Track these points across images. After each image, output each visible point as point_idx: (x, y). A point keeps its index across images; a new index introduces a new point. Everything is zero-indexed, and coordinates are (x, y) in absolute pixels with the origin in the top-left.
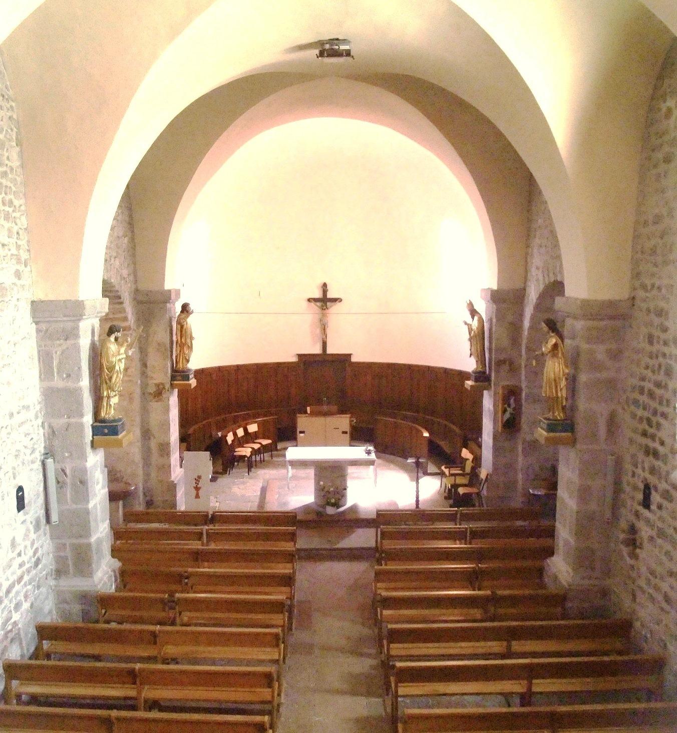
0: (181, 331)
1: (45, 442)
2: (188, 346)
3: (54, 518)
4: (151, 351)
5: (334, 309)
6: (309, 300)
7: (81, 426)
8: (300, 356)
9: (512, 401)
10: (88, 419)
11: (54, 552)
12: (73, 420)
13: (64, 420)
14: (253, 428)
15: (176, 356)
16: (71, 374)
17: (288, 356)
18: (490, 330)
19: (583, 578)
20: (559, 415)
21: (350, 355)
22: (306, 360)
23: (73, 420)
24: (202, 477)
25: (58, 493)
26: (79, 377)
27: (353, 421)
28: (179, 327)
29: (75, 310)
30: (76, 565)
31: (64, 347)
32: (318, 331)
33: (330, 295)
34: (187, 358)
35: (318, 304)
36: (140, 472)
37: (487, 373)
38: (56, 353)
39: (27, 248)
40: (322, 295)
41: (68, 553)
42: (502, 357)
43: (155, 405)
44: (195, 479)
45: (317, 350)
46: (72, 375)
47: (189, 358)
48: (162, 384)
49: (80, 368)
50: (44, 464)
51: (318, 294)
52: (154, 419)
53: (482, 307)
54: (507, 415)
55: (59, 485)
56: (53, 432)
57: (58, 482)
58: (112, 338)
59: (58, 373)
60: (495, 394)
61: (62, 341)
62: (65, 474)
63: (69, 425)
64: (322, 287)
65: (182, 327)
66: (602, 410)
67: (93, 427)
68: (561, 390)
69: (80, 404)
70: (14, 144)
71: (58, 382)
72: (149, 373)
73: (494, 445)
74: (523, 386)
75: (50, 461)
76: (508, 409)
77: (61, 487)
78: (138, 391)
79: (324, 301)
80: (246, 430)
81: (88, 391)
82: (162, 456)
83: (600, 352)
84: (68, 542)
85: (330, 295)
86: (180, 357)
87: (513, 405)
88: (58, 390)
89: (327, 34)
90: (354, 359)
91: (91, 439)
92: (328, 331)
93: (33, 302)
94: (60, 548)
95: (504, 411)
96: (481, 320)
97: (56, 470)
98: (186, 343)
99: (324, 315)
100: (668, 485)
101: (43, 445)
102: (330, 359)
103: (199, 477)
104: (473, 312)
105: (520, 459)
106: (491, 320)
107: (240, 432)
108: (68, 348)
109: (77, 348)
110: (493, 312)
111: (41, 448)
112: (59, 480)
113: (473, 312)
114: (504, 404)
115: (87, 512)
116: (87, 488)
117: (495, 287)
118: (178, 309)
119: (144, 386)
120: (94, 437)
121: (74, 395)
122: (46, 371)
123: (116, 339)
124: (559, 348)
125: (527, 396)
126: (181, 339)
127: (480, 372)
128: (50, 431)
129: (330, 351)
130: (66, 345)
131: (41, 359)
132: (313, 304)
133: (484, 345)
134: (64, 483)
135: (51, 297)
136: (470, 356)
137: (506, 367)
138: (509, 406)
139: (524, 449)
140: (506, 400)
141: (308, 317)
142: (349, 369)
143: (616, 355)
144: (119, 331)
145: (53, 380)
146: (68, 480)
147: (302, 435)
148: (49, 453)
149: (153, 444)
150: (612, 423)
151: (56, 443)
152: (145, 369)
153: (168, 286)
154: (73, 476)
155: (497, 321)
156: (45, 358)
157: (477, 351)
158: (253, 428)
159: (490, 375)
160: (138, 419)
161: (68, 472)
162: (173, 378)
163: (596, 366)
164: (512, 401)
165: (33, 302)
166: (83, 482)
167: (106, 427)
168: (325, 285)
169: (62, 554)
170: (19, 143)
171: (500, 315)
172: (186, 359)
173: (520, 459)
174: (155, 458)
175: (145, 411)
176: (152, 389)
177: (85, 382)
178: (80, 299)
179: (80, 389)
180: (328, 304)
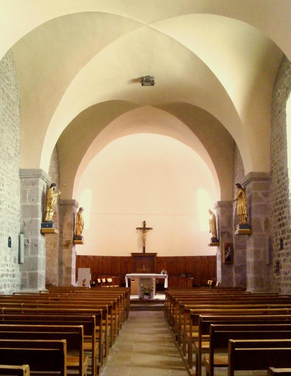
0: (79, 218)
1: (21, 228)
2: (82, 225)
3: (22, 260)
4: (65, 225)
5: (149, 233)
6: (137, 229)
7: (37, 221)
8: (133, 254)
9: (229, 249)
10: (40, 219)
11: (21, 277)
12: (33, 219)
13: (30, 219)
14: (110, 280)
15: (76, 230)
16: (34, 199)
17: (127, 254)
18: (219, 220)
19: (258, 291)
20: (244, 222)
21: (156, 253)
22: (135, 255)
23: (33, 219)
24: (86, 280)
25: (25, 250)
26: (37, 201)
27: (158, 281)
28: (78, 216)
29: (38, 174)
30: (30, 282)
31: (32, 188)
32: (141, 242)
33: (147, 226)
34: (81, 231)
35: (142, 230)
36: (57, 279)
37: (218, 239)
38: (28, 191)
39: (20, 140)
40: (143, 226)
41: (27, 277)
42: (224, 230)
43: (65, 250)
44: (83, 281)
45: (141, 251)
46: (35, 200)
47: (82, 231)
48: (69, 241)
49: (38, 197)
50: (19, 236)
51: (141, 226)
52: (65, 256)
53: (215, 212)
54: (227, 255)
55: (25, 247)
56: (25, 224)
57: (25, 245)
58: (52, 189)
59: (29, 199)
60: (222, 247)
61: (31, 186)
62: (28, 242)
63: (32, 221)
64: (143, 223)
65: (79, 216)
66: (262, 218)
67: (42, 224)
68: (244, 211)
69: (37, 211)
70: (18, 106)
71: (28, 203)
72: (64, 236)
73: (222, 270)
74: (234, 242)
75: (22, 236)
76: (227, 252)
77: (26, 248)
78: (58, 244)
79: (144, 229)
80: (106, 280)
81: (41, 208)
82: (67, 274)
83: (260, 194)
84: (27, 272)
85: (147, 226)
86: (78, 229)
87: (230, 251)
88: (28, 206)
89: (145, 75)
90: (158, 255)
91: (40, 229)
92: (146, 242)
93: (20, 170)
94: (24, 275)
95: (226, 253)
96: (214, 216)
97: (24, 240)
98: (80, 224)
99: (144, 235)
100: (289, 233)
101: (19, 229)
102: (147, 255)
103: (85, 280)
104: (211, 213)
105: (234, 274)
106: (219, 216)
107: (104, 280)
108: (33, 189)
109: (38, 189)
110: (219, 212)
111: (18, 230)
112: (26, 245)
113: (211, 213)
114: (225, 250)
115: (37, 259)
116: (38, 248)
117: (220, 200)
118: (77, 210)
119: (61, 242)
120: (42, 228)
121: (34, 208)
122: (23, 198)
123: (54, 189)
124: (243, 195)
125: (236, 246)
126: (79, 221)
127: (214, 238)
128: (23, 223)
129: (147, 252)
130: (32, 187)
131: (22, 193)
132: (139, 231)
133: (216, 228)
134: (28, 246)
135: (28, 168)
136: (210, 232)
137: (226, 235)
138: (228, 251)
139: (235, 270)
140: (226, 249)
141: (138, 235)
142: (156, 261)
143: (266, 195)
144: (55, 186)
145: (26, 202)
146: (30, 244)
147: (133, 282)
148: (22, 233)
149: (64, 268)
150: (267, 222)
151: (26, 228)
152: (61, 234)
153: (73, 198)
154: (32, 243)
155: (221, 215)
156: (23, 193)
157: (213, 231)
158: (110, 280)
159: (219, 240)
160: (57, 255)
161: (30, 241)
162: (74, 239)
163: (259, 199)
164: (229, 249)
165: (20, 170)
166: (36, 245)
167: (47, 224)
168: (145, 222)
169: (24, 278)
170: (20, 107)
171: (222, 213)
172: (80, 231)
173: (234, 274)
174: (64, 274)
175: (60, 253)
176: (64, 243)
177: (40, 204)
178: (40, 169)
179: (38, 205)
180: (146, 230)
